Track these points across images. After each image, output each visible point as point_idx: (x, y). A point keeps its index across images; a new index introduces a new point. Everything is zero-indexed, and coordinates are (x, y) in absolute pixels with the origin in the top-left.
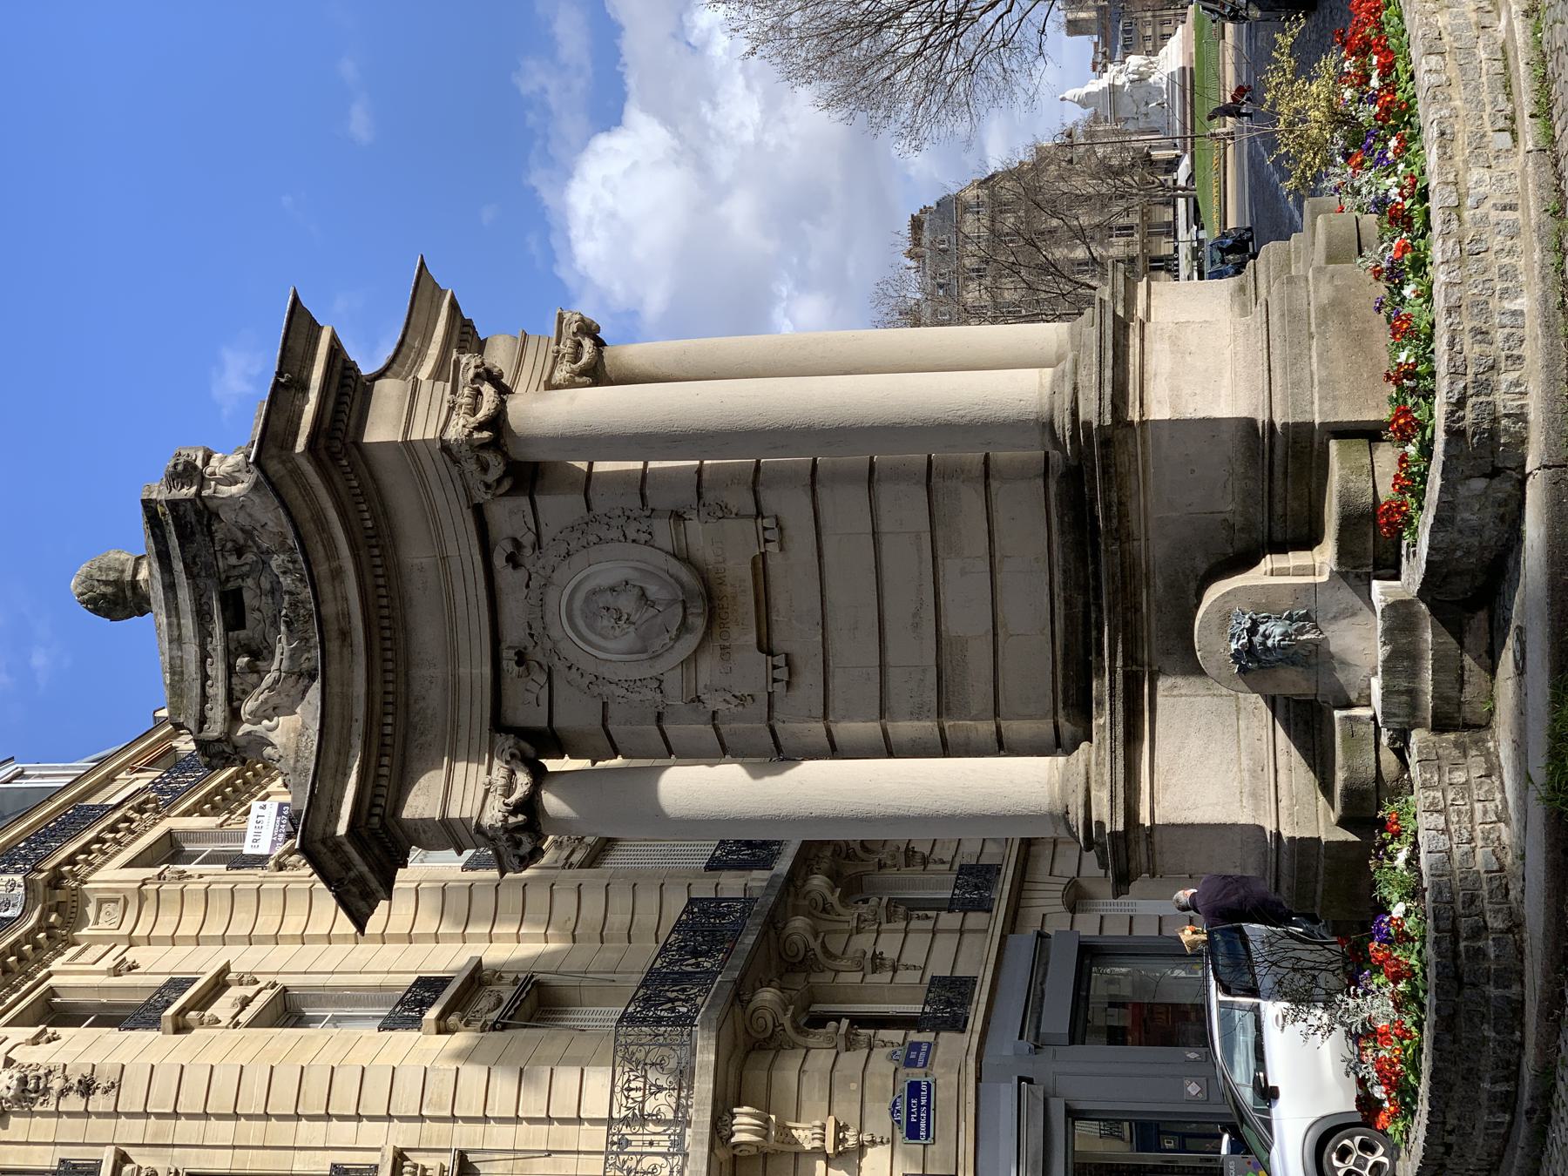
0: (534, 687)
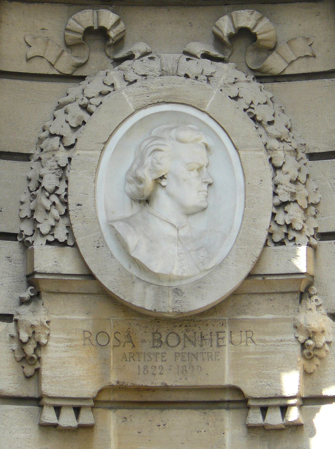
0: (51, 55)
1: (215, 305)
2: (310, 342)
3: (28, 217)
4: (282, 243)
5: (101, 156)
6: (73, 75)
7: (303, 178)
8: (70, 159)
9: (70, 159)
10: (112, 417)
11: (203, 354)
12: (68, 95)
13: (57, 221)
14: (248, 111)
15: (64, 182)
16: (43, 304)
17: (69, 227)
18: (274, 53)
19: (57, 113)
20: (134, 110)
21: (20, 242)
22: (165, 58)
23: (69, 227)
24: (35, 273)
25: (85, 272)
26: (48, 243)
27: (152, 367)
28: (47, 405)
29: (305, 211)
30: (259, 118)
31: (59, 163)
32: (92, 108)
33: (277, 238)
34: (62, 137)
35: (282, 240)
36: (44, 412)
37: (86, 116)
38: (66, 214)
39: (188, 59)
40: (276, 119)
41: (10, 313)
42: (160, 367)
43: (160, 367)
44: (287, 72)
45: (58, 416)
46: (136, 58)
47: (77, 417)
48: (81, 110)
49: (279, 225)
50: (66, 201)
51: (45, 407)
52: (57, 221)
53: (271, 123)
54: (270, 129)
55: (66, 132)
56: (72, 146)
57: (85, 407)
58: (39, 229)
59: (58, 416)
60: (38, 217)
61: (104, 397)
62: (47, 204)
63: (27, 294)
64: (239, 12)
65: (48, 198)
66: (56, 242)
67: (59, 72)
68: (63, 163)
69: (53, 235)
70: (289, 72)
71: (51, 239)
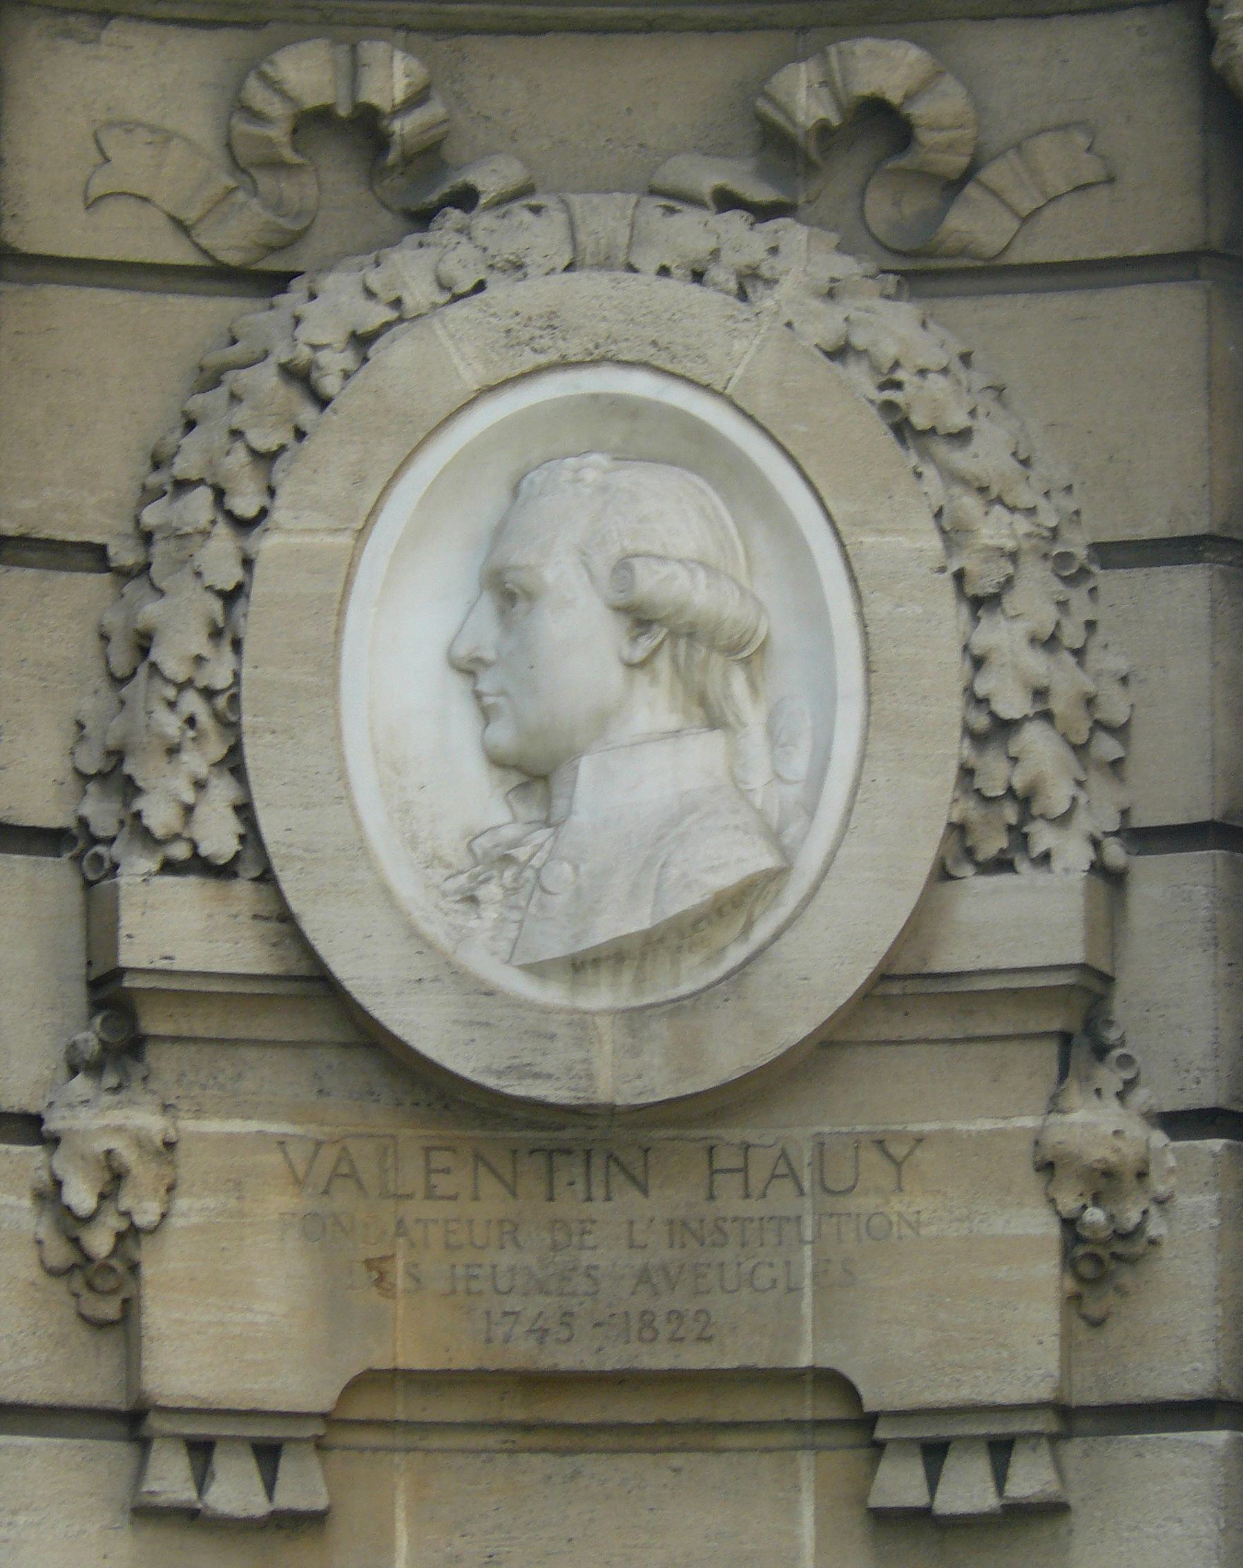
2: (1095, 1215)
7: (1073, 635)
8: (480, 287)
10: (402, 1484)
12: (234, 341)
13: (200, 785)
15: (227, 649)
16: (145, 1079)
17: (244, 810)
18: (971, 190)
19: (197, 403)
23: (244, 810)
24: (119, 973)
25: (301, 967)
26: (169, 867)
27: (671, 1312)
28: (165, 1436)
29: (1080, 750)
30: (920, 420)
31: (209, 579)
33: (993, 844)
36: (187, 1481)
37: (307, 414)
39: (671, 211)
40: (981, 424)
41: (32, 1110)
42: (674, 1317)
43: (703, 1318)
44: (1015, 257)
46: (482, 201)
47: (270, 1488)
49: (988, 800)
50: (233, 719)
51: (156, 1445)
52: (200, 785)
53: (962, 437)
54: (959, 459)
61: (366, 1407)
62: (171, 725)
64: (845, 45)
65: (172, 705)
68: (229, 576)
70: (1022, 254)
71: (180, 851)
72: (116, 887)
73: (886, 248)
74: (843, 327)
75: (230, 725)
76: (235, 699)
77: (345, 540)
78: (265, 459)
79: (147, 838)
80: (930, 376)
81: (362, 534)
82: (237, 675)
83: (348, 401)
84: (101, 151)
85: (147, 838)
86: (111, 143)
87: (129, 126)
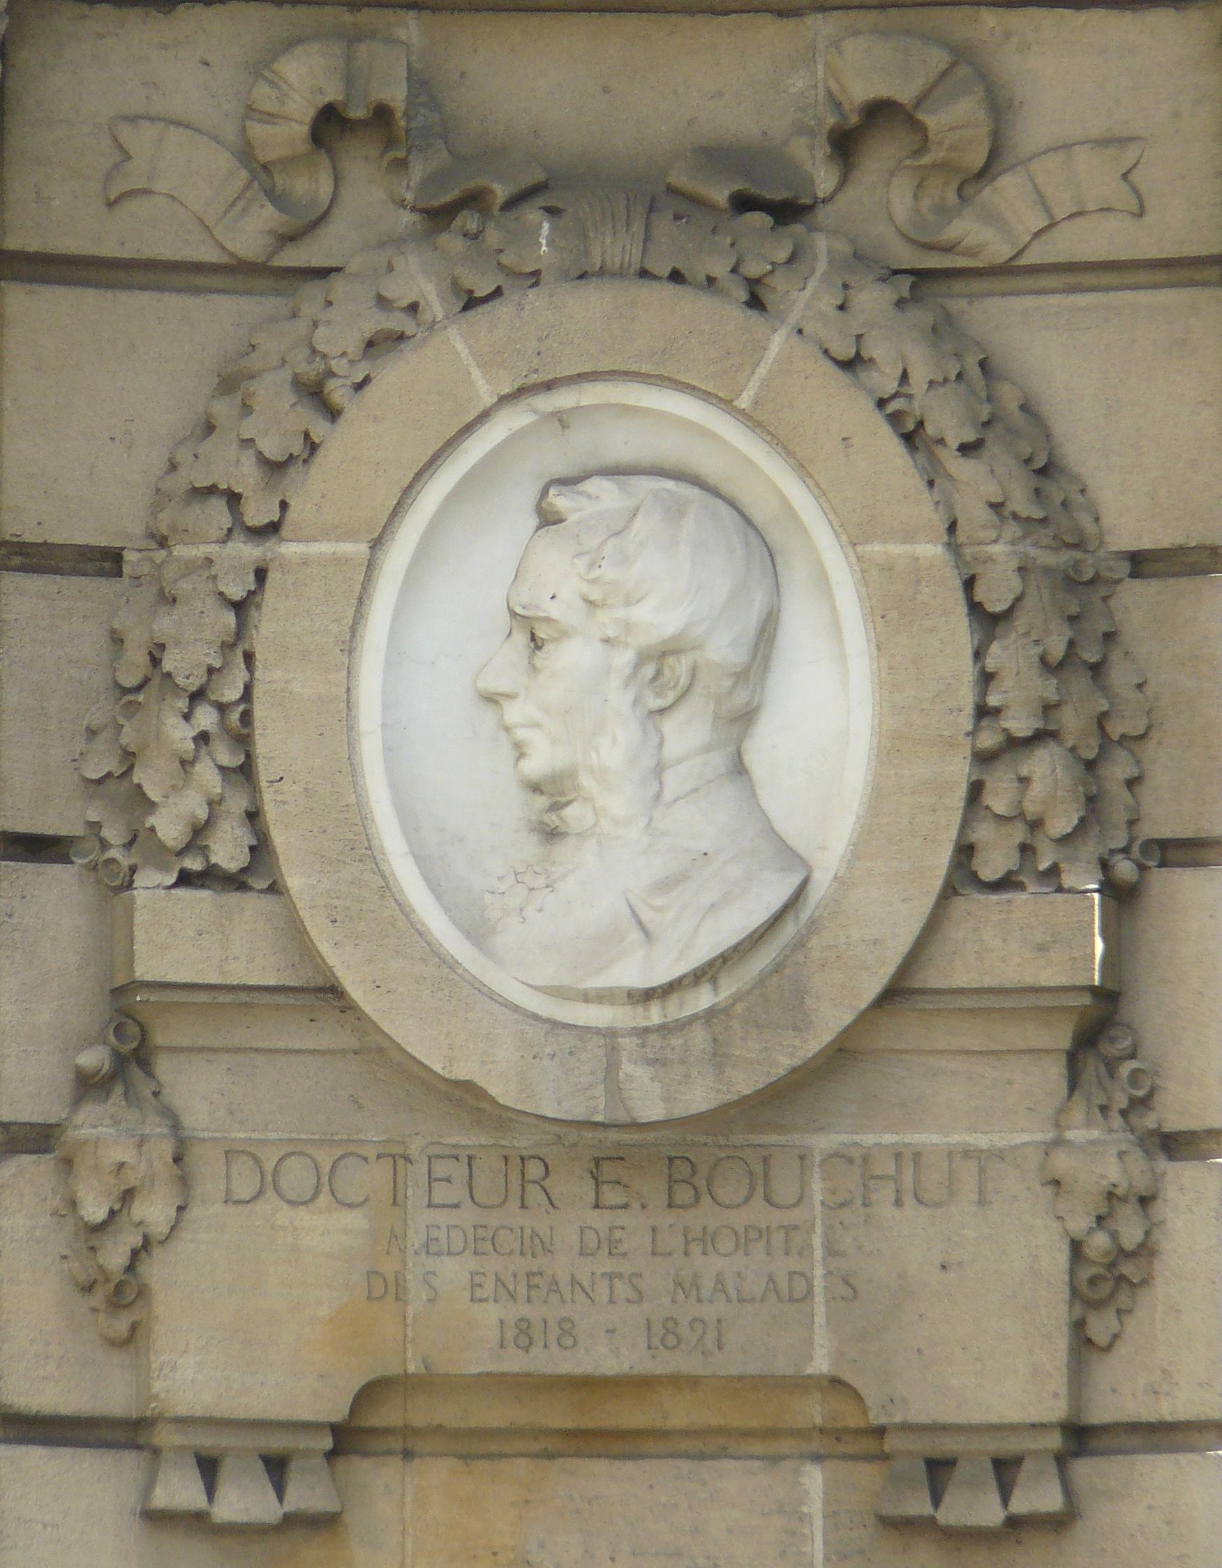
1: (1183, 1129)
3: (116, 775)
4: (1005, 883)
5: (371, 566)
6: (276, 264)
9: (261, 574)
11: (1101, 1412)
14: (892, 407)
20: (489, 400)
21: (85, 866)
22: (271, 755)
26: (185, 879)
32: (337, 392)
33: (992, 865)
34: (233, 498)
35: (1010, 873)
38: (245, 772)
43: (699, 1326)
45: (210, 1490)
47: (280, 1493)
48: (299, 408)
50: (245, 731)
55: (246, 477)
56: (273, 528)
57: (307, 1453)
58: (152, 829)
59: (210, 1490)
60: (150, 779)
63: (94, 1058)
65: (187, 717)
66: (209, 878)
67: (223, 248)
69: (205, 851)
71: (194, 864)
72: (133, 899)
73: (913, 242)
74: (78, 831)
75: (243, 739)
76: (246, 717)
77: (363, 548)
78: (275, 468)
79: (160, 854)
80: (404, 303)
81: (377, 544)
82: (248, 689)
83: (350, 413)
84: (120, 147)
85: (160, 854)
86: (126, 134)
87: (132, 119)
